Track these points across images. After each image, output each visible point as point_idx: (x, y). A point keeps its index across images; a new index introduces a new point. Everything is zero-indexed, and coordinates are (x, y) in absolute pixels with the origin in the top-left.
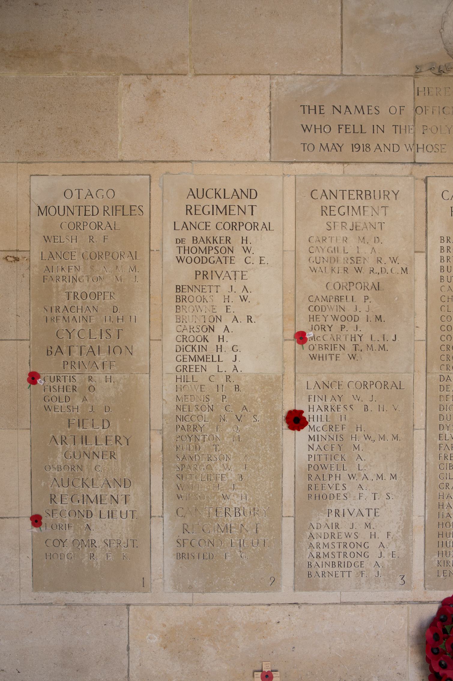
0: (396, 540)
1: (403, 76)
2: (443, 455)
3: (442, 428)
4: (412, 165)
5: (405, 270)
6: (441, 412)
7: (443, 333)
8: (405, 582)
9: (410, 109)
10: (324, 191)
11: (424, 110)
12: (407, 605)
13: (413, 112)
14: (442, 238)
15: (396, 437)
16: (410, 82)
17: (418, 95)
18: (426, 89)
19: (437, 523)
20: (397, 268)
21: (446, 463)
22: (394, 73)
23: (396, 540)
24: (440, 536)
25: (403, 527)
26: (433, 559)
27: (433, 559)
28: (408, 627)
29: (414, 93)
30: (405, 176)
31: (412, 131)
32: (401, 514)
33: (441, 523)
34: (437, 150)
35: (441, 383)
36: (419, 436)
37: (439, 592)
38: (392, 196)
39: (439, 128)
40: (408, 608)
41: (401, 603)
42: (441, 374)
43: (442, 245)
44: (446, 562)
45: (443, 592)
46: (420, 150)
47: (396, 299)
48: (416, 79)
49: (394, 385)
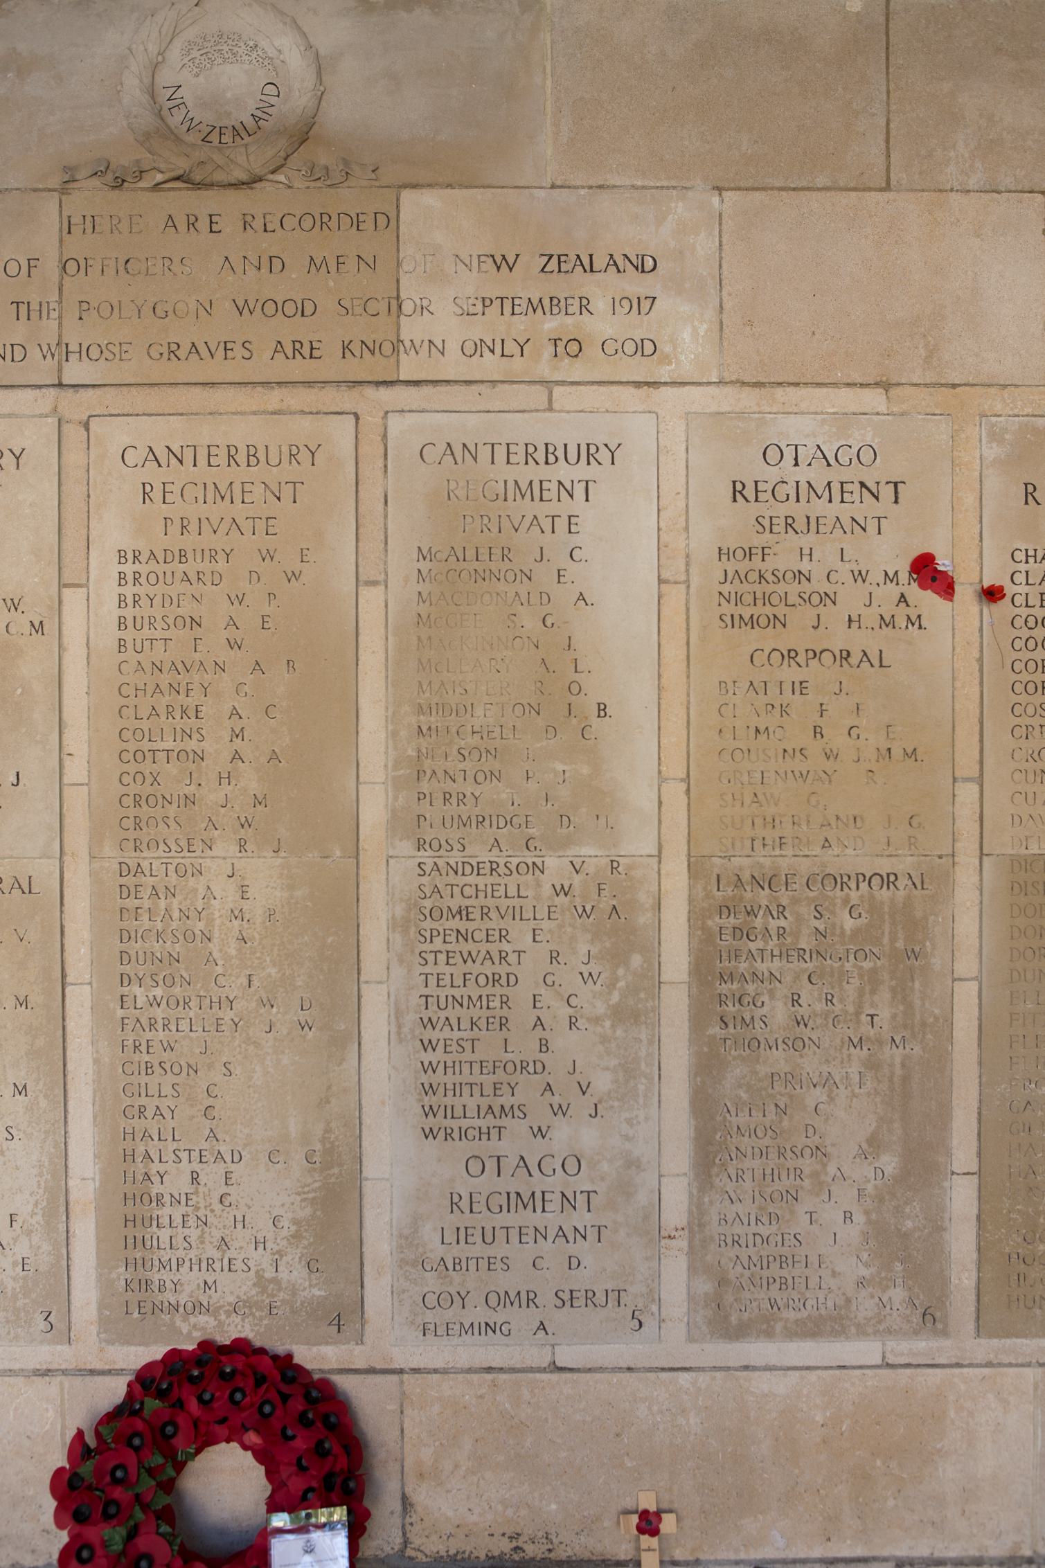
0: (29, 1233)
1: (35, 190)
2: (131, 1041)
3: (126, 982)
4: (57, 390)
5: (38, 628)
6: (123, 947)
7: (126, 767)
8: (58, 1326)
9: (50, 265)
10: (449, 444)
11: (84, 266)
12: (59, 1378)
13: (57, 271)
14: (123, 554)
15: (23, 1002)
16: (50, 205)
17: (69, 232)
18: (89, 219)
19: (122, 1196)
20: (21, 623)
21: (137, 1059)
22: (16, 186)
23: (29, 1233)
24: (130, 1224)
25: (45, 1204)
26: (114, 1275)
27: (114, 1275)
28: (64, 1427)
29: (61, 230)
30: (41, 416)
31: (54, 315)
32: (40, 1175)
33: (130, 1196)
34: (111, 356)
35: (123, 881)
36: (80, 999)
37: (133, 1348)
38: (604, 455)
39: (116, 305)
40: (61, 1383)
41: (47, 1373)
42: (122, 860)
43: (122, 568)
44: (143, 1282)
45: (142, 1348)
46: (73, 358)
47: (19, 691)
48: (64, 198)
49: (16, 885)
